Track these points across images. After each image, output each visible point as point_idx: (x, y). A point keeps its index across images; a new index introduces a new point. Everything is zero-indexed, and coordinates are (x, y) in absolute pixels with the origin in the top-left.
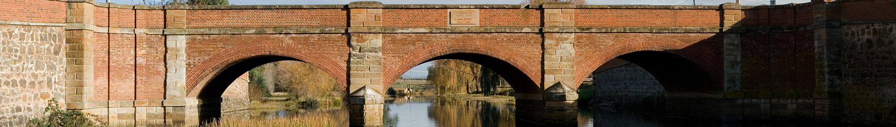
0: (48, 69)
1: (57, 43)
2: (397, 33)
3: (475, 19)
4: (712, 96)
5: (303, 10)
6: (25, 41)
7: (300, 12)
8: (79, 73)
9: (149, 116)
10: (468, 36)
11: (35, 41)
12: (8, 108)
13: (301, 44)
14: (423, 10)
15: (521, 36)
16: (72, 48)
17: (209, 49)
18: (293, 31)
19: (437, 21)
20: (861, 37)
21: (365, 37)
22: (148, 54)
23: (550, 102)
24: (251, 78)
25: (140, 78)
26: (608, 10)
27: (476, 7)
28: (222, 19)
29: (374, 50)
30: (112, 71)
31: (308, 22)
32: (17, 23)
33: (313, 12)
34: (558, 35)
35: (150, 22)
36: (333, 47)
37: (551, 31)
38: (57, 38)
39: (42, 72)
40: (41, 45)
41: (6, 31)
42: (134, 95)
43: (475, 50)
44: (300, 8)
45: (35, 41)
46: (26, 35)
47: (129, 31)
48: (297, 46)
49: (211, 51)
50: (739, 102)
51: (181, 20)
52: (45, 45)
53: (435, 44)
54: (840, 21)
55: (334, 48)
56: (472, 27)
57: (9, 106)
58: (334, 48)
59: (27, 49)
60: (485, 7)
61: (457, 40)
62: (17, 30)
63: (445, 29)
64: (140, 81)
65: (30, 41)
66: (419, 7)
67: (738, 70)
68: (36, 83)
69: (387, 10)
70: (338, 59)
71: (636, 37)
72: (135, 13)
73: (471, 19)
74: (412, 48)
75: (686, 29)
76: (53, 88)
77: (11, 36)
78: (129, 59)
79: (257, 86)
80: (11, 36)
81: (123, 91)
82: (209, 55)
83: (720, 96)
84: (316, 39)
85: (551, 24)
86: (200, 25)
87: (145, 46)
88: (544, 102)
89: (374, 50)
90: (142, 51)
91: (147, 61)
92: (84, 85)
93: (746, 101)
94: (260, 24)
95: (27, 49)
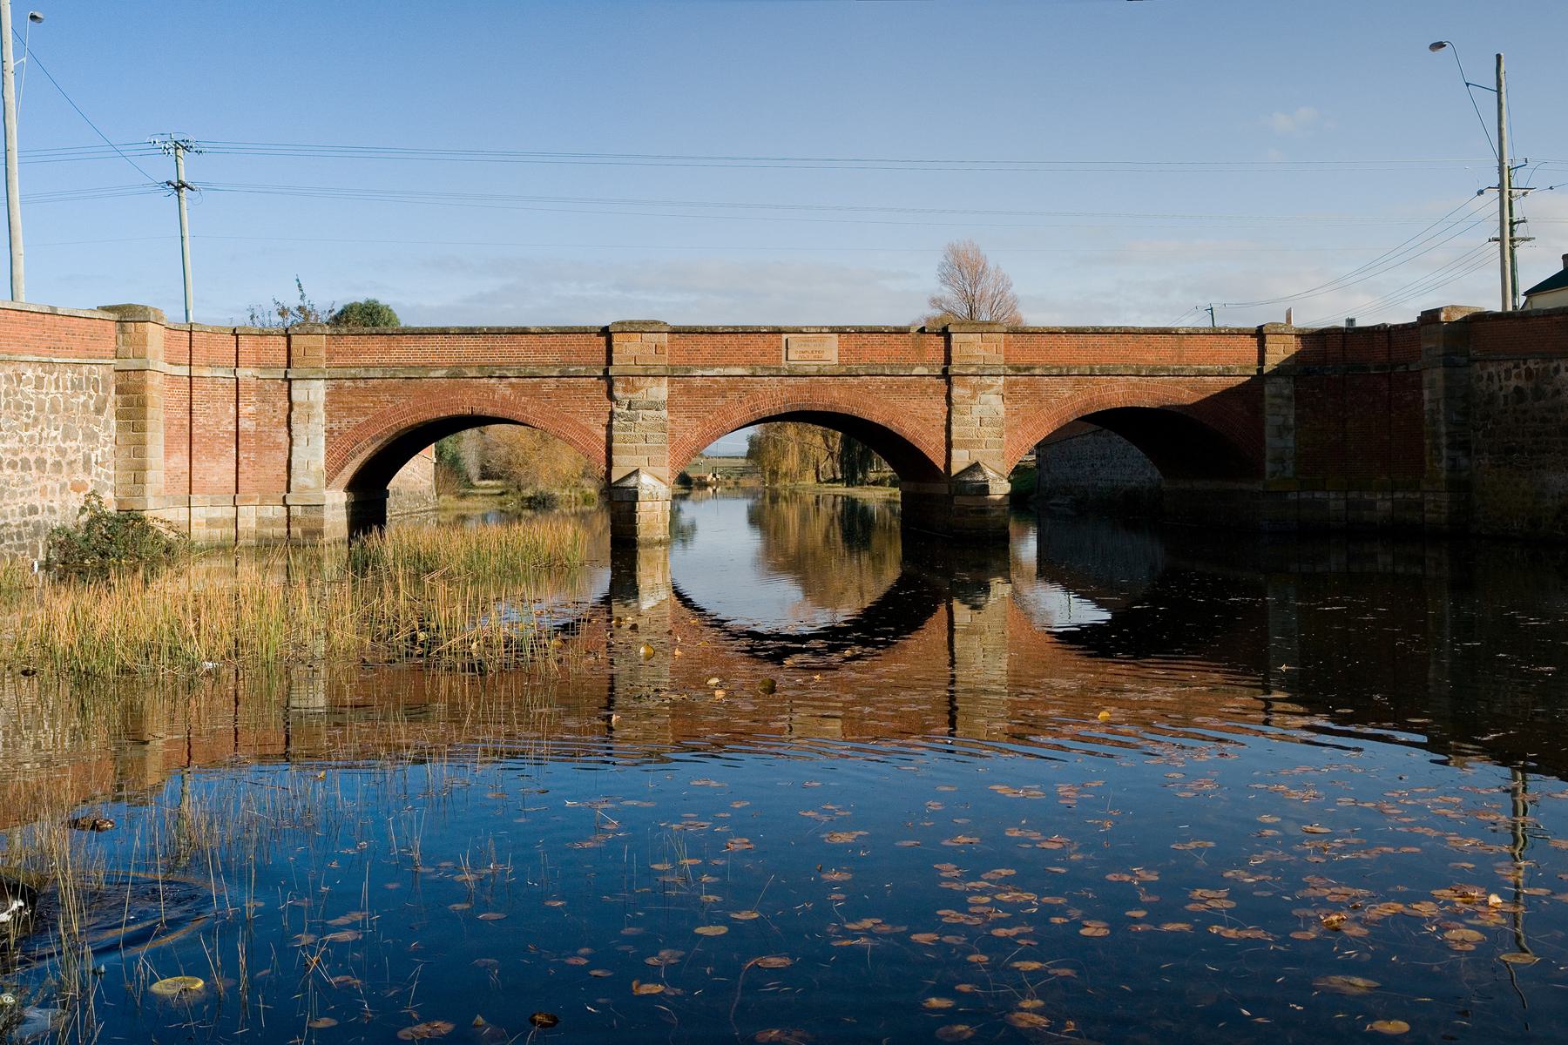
2: (695, 376)
3: (831, 352)
4: (1244, 486)
5: (530, 336)
6: (44, 391)
7: (524, 339)
8: (139, 447)
9: (261, 522)
11: (61, 391)
13: (526, 396)
14: (740, 335)
16: (127, 403)
21: (638, 382)
22: (259, 412)
24: (439, 454)
25: (246, 456)
26: (1063, 336)
31: (539, 357)
32: (30, 358)
33: (548, 339)
34: (975, 380)
36: (582, 400)
37: (964, 372)
39: (74, 444)
45: (61, 391)
50: (1292, 497)
57: (16, 504)
59: (47, 405)
60: (848, 330)
61: (799, 388)
63: (779, 369)
64: (246, 461)
70: (592, 423)
72: (237, 340)
74: (720, 402)
75: (1199, 370)
76: (93, 472)
81: (216, 478)
82: (366, 414)
83: (1259, 487)
86: (350, 361)
88: (950, 498)
89: (654, 406)
90: (250, 408)
91: (258, 425)
92: (148, 467)
94: (456, 361)
95: (47, 405)
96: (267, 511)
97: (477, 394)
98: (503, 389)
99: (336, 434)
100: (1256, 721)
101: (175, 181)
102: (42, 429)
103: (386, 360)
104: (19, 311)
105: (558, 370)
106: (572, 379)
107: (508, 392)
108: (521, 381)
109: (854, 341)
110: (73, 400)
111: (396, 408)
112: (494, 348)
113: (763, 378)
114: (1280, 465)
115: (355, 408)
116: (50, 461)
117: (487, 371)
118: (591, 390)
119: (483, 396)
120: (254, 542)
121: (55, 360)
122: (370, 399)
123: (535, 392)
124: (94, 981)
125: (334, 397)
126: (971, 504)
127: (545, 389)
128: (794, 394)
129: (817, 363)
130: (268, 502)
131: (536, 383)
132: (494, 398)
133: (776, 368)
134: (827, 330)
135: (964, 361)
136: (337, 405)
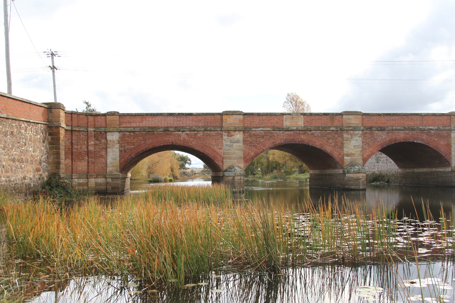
1: (44, 135)
2: (253, 131)
4: (441, 170)
5: (193, 117)
6: (27, 132)
7: (191, 118)
9: (96, 184)
10: (296, 133)
11: (33, 133)
12: (19, 177)
13: (192, 138)
14: (269, 116)
15: (329, 133)
16: (52, 139)
17: (134, 141)
18: (187, 129)
19: (277, 123)
21: (232, 133)
22: (95, 145)
23: (349, 174)
25: (91, 160)
26: (382, 117)
28: (142, 122)
29: (238, 141)
30: (74, 155)
32: (24, 119)
33: (200, 117)
35: (96, 124)
37: (348, 129)
40: (36, 136)
42: (56, 77)
43: (435, 146)
44: (191, 114)
45: (33, 133)
46: (28, 128)
47: (84, 129)
48: (190, 139)
49: (135, 142)
51: (116, 122)
52: (38, 136)
53: (276, 138)
56: (299, 127)
60: (307, 114)
61: (290, 135)
62: (77, 181)
63: (283, 128)
64: (91, 162)
65: (30, 133)
69: (246, 116)
70: (216, 148)
71: (399, 133)
72: (72, 117)
74: (262, 140)
75: (429, 128)
76: (42, 165)
77: (20, 128)
78: (84, 147)
80: (20, 128)
81: (81, 168)
82: (134, 145)
83: (449, 169)
84: (202, 135)
85: (348, 125)
86: (128, 125)
87: (94, 139)
89: (238, 141)
90: (92, 142)
91: (95, 148)
92: (61, 163)
94: (166, 125)
96: (99, 180)
97: (174, 137)
98: (183, 135)
99: (123, 152)
101: (51, 66)
103: (141, 125)
104: (58, 108)
105: (203, 128)
106: (209, 132)
110: (36, 137)
112: (180, 120)
113: (277, 131)
114: (292, 185)
115: (130, 142)
116: (29, 160)
117: (178, 129)
118: (215, 136)
119: (176, 138)
122: (135, 139)
125: (122, 141)
126: (354, 177)
127: (199, 135)
129: (296, 126)
130: (99, 177)
131: (196, 133)
132: (180, 138)
133: (282, 128)
134: (300, 114)
136: (123, 141)
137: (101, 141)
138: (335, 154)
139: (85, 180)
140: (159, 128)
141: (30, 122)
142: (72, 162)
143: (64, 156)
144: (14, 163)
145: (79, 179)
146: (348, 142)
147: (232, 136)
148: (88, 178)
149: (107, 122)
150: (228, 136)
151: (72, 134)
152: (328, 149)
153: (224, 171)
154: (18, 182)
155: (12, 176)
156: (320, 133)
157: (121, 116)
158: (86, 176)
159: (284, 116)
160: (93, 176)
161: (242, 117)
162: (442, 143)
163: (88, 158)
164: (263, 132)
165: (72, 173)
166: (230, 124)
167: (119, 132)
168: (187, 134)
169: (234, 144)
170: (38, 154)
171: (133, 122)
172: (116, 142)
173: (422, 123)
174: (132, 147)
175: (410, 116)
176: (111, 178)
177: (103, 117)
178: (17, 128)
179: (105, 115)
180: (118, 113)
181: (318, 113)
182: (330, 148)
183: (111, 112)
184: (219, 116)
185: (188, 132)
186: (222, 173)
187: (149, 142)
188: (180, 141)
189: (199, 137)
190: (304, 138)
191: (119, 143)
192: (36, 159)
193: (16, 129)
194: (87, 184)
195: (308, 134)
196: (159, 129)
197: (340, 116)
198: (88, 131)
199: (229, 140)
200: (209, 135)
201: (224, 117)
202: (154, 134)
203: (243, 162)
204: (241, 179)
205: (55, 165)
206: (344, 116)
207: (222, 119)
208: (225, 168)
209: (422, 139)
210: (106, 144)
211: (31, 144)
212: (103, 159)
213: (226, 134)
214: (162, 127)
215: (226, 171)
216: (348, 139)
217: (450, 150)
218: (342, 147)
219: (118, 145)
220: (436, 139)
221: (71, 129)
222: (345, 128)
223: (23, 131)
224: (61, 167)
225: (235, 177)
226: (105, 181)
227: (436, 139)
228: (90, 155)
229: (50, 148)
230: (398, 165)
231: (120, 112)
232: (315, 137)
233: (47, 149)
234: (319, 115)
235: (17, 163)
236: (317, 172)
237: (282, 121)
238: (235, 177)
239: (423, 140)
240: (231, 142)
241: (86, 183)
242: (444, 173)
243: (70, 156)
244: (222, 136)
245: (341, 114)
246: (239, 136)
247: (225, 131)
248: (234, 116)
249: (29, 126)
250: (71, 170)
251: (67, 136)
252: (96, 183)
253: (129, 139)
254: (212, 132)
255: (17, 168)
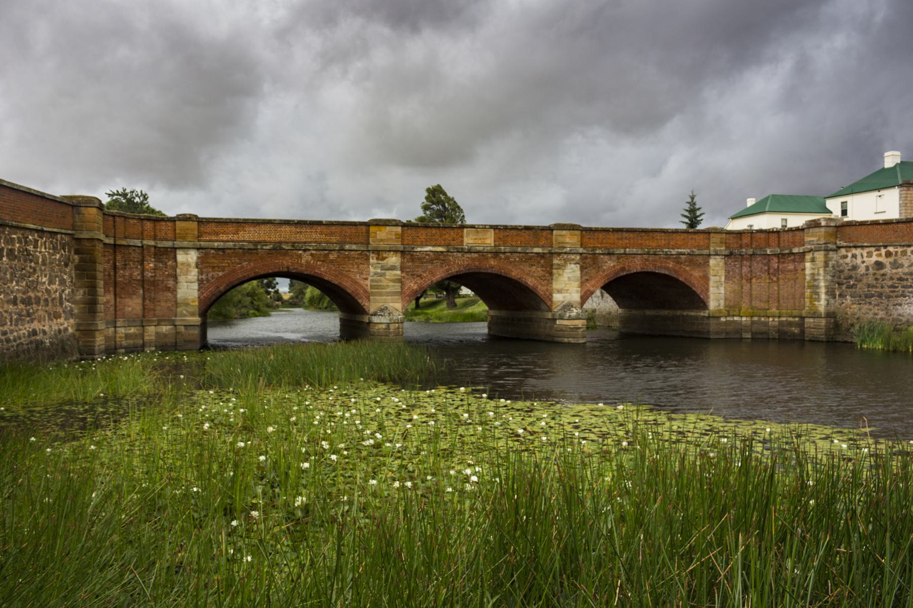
0: (58, 285)
3: (489, 240)
4: (692, 314)
6: (39, 250)
7: (319, 229)
8: (92, 289)
12: (24, 331)
19: (454, 240)
20: (865, 259)
22: (155, 269)
24: (802, 68)
27: (491, 227)
28: (237, 233)
29: (393, 268)
31: (328, 238)
32: (32, 226)
33: (333, 228)
34: (565, 256)
36: (352, 264)
38: (682, 250)
39: (54, 287)
41: (20, 236)
44: (319, 223)
50: (723, 319)
54: (836, 243)
55: (353, 265)
57: (25, 329)
58: (353, 265)
59: (40, 260)
61: (473, 259)
65: (43, 250)
66: (723, 336)
67: (722, 290)
68: (49, 299)
69: (406, 228)
72: (115, 222)
73: (486, 238)
74: (430, 266)
77: (26, 242)
79: (775, 291)
81: (130, 309)
82: (223, 271)
84: (336, 256)
86: (214, 238)
87: (153, 260)
88: (554, 320)
89: (393, 268)
93: (728, 319)
94: (278, 239)
95: (40, 260)
100: (681, 232)
102: (38, 277)
103: (236, 238)
107: (310, 258)
108: (318, 253)
109: (502, 234)
111: (242, 267)
112: (301, 232)
120: (124, 335)
121: (45, 229)
123: (325, 259)
124: (568, 531)
125: (201, 264)
127: (331, 257)
128: (470, 262)
130: (163, 323)
135: (560, 245)
137: (166, 264)
138: (541, 289)
139: (138, 330)
140: (265, 243)
141: (42, 231)
142: (115, 299)
143: (102, 290)
144: (15, 307)
145: (128, 328)
146: (560, 271)
147: (384, 259)
148: (143, 326)
149: (177, 231)
150: (377, 259)
151: (115, 252)
152: (530, 282)
153: (372, 315)
154: (23, 340)
155: (12, 331)
156: (518, 257)
157: (202, 222)
158: (138, 323)
159: (465, 230)
160: (152, 321)
161: (399, 229)
162: (697, 273)
163: (144, 291)
164: (431, 254)
165: (116, 318)
166: (382, 240)
167: (198, 249)
168: (312, 255)
169: (388, 273)
170: (58, 287)
171: (223, 233)
172: (193, 265)
173: (669, 244)
174: (221, 274)
175: (651, 234)
176: (184, 326)
177: (169, 224)
178: (20, 242)
179: (173, 220)
180: (196, 216)
181: (516, 226)
182: (533, 280)
183: (185, 215)
184: (364, 228)
185: (314, 252)
186: (367, 316)
187: (249, 267)
188: (301, 265)
189: (332, 260)
190: (493, 265)
191: (197, 267)
192: (53, 296)
193: (18, 245)
194: (142, 336)
195: (501, 259)
196: (266, 245)
197: (548, 232)
198: (142, 247)
199: (380, 265)
200: (348, 257)
201: (372, 229)
202: (258, 254)
203: (400, 301)
204: (398, 328)
205: (87, 306)
206: (555, 232)
207: (368, 232)
208: (372, 311)
209: (668, 267)
210: (175, 268)
211: (45, 270)
212: (170, 294)
213: (375, 256)
214: (270, 242)
215: (375, 314)
216: (560, 267)
217: (708, 284)
218: (550, 282)
219: (196, 270)
220: (688, 268)
221: (113, 243)
222: (556, 250)
223: (31, 248)
224: (99, 310)
225: (391, 325)
226: (174, 331)
227: (688, 268)
228: (146, 286)
229: (77, 275)
230: (618, 304)
231: (200, 216)
232: (511, 262)
233: (72, 278)
234: (518, 229)
235: (21, 306)
236: (503, 313)
237: (462, 237)
238: (391, 325)
239: (668, 268)
240: (383, 268)
241: (140, 334)
242: (696, 318)
243: (112, 289)
244: (368, 259)
245: (550, 229)
246: (394, 260)
247: (374, 251)
248: (388, 228)
249: (42, 238)
250: (113, 312)
251: (106, 254)
252: (157, 333)
253: (216, 261)
254: (352, 253)
255: (20, 315)
